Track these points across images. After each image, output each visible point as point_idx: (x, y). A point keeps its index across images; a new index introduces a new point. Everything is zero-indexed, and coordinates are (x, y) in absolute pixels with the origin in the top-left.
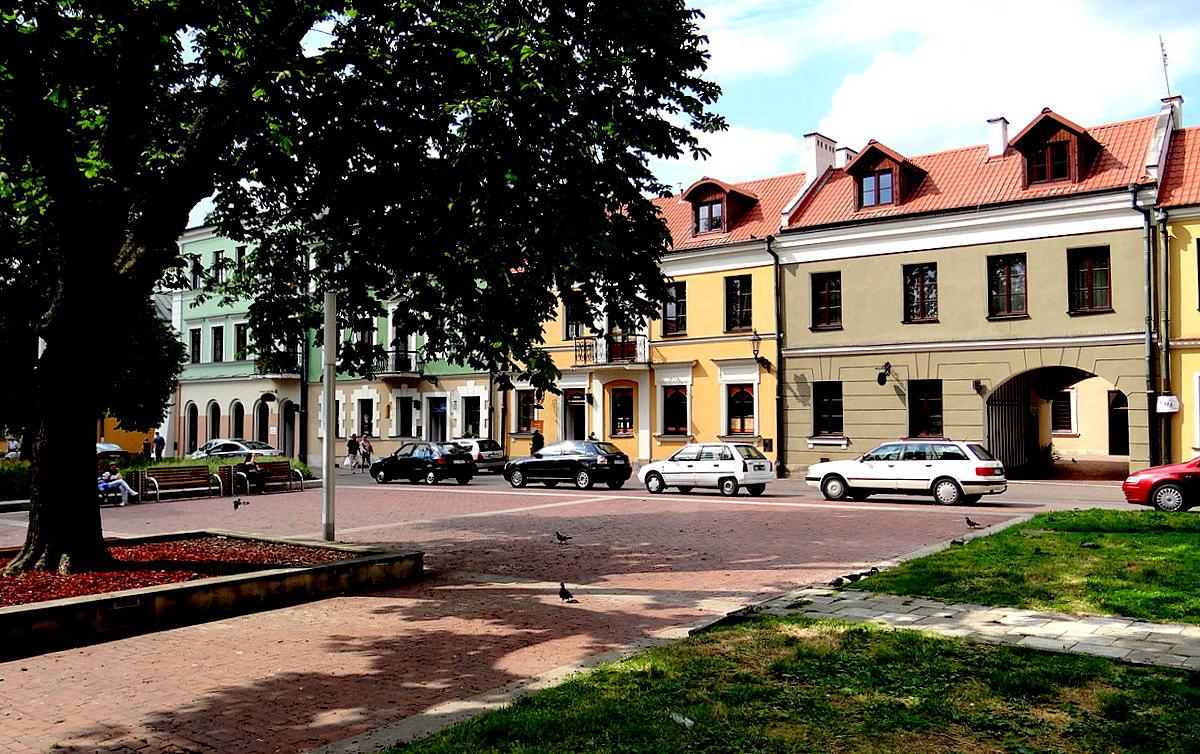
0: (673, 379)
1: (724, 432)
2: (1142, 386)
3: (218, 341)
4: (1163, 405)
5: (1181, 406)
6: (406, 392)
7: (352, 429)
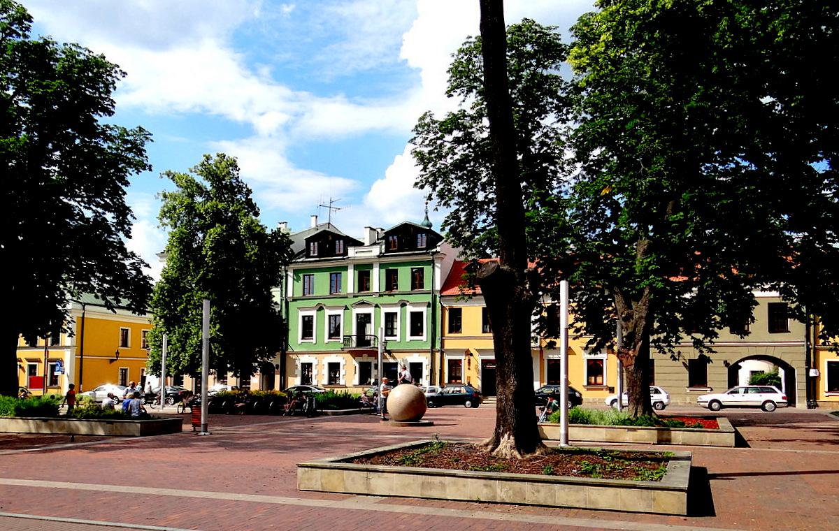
0: (555, 356)
1: (586, 384)
2: (803, 364)
3: (390, 324)
4: (812, 373)
5: (820, 373)
6: (365, 359)
7: (323, 380)
